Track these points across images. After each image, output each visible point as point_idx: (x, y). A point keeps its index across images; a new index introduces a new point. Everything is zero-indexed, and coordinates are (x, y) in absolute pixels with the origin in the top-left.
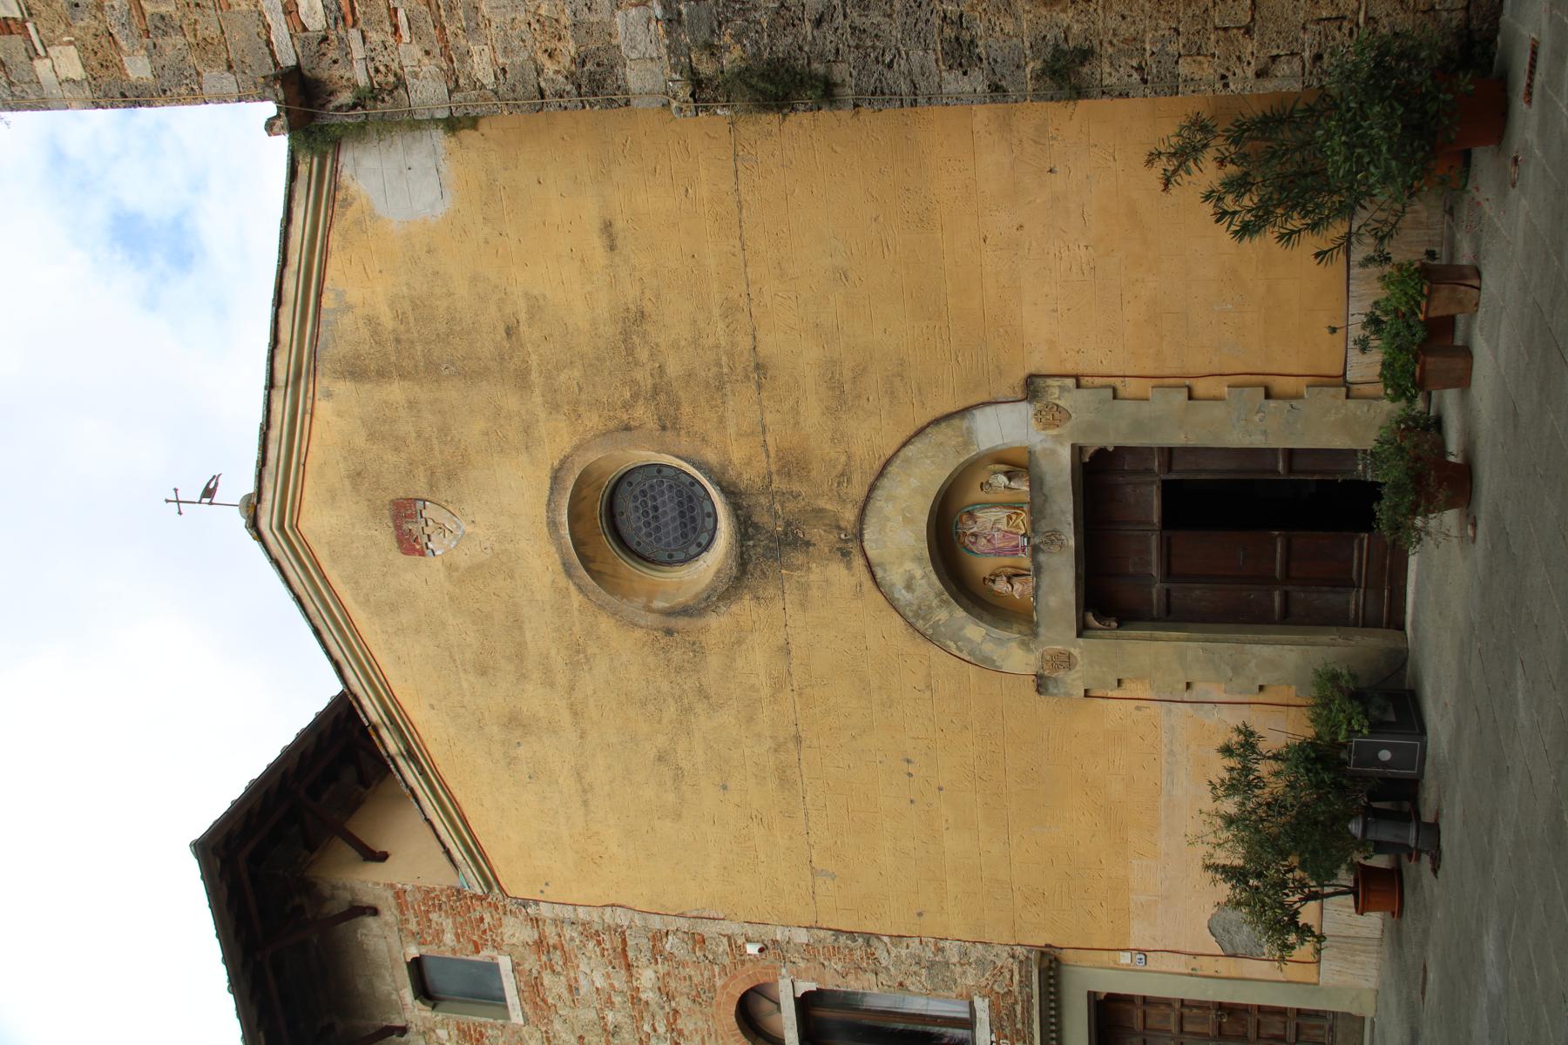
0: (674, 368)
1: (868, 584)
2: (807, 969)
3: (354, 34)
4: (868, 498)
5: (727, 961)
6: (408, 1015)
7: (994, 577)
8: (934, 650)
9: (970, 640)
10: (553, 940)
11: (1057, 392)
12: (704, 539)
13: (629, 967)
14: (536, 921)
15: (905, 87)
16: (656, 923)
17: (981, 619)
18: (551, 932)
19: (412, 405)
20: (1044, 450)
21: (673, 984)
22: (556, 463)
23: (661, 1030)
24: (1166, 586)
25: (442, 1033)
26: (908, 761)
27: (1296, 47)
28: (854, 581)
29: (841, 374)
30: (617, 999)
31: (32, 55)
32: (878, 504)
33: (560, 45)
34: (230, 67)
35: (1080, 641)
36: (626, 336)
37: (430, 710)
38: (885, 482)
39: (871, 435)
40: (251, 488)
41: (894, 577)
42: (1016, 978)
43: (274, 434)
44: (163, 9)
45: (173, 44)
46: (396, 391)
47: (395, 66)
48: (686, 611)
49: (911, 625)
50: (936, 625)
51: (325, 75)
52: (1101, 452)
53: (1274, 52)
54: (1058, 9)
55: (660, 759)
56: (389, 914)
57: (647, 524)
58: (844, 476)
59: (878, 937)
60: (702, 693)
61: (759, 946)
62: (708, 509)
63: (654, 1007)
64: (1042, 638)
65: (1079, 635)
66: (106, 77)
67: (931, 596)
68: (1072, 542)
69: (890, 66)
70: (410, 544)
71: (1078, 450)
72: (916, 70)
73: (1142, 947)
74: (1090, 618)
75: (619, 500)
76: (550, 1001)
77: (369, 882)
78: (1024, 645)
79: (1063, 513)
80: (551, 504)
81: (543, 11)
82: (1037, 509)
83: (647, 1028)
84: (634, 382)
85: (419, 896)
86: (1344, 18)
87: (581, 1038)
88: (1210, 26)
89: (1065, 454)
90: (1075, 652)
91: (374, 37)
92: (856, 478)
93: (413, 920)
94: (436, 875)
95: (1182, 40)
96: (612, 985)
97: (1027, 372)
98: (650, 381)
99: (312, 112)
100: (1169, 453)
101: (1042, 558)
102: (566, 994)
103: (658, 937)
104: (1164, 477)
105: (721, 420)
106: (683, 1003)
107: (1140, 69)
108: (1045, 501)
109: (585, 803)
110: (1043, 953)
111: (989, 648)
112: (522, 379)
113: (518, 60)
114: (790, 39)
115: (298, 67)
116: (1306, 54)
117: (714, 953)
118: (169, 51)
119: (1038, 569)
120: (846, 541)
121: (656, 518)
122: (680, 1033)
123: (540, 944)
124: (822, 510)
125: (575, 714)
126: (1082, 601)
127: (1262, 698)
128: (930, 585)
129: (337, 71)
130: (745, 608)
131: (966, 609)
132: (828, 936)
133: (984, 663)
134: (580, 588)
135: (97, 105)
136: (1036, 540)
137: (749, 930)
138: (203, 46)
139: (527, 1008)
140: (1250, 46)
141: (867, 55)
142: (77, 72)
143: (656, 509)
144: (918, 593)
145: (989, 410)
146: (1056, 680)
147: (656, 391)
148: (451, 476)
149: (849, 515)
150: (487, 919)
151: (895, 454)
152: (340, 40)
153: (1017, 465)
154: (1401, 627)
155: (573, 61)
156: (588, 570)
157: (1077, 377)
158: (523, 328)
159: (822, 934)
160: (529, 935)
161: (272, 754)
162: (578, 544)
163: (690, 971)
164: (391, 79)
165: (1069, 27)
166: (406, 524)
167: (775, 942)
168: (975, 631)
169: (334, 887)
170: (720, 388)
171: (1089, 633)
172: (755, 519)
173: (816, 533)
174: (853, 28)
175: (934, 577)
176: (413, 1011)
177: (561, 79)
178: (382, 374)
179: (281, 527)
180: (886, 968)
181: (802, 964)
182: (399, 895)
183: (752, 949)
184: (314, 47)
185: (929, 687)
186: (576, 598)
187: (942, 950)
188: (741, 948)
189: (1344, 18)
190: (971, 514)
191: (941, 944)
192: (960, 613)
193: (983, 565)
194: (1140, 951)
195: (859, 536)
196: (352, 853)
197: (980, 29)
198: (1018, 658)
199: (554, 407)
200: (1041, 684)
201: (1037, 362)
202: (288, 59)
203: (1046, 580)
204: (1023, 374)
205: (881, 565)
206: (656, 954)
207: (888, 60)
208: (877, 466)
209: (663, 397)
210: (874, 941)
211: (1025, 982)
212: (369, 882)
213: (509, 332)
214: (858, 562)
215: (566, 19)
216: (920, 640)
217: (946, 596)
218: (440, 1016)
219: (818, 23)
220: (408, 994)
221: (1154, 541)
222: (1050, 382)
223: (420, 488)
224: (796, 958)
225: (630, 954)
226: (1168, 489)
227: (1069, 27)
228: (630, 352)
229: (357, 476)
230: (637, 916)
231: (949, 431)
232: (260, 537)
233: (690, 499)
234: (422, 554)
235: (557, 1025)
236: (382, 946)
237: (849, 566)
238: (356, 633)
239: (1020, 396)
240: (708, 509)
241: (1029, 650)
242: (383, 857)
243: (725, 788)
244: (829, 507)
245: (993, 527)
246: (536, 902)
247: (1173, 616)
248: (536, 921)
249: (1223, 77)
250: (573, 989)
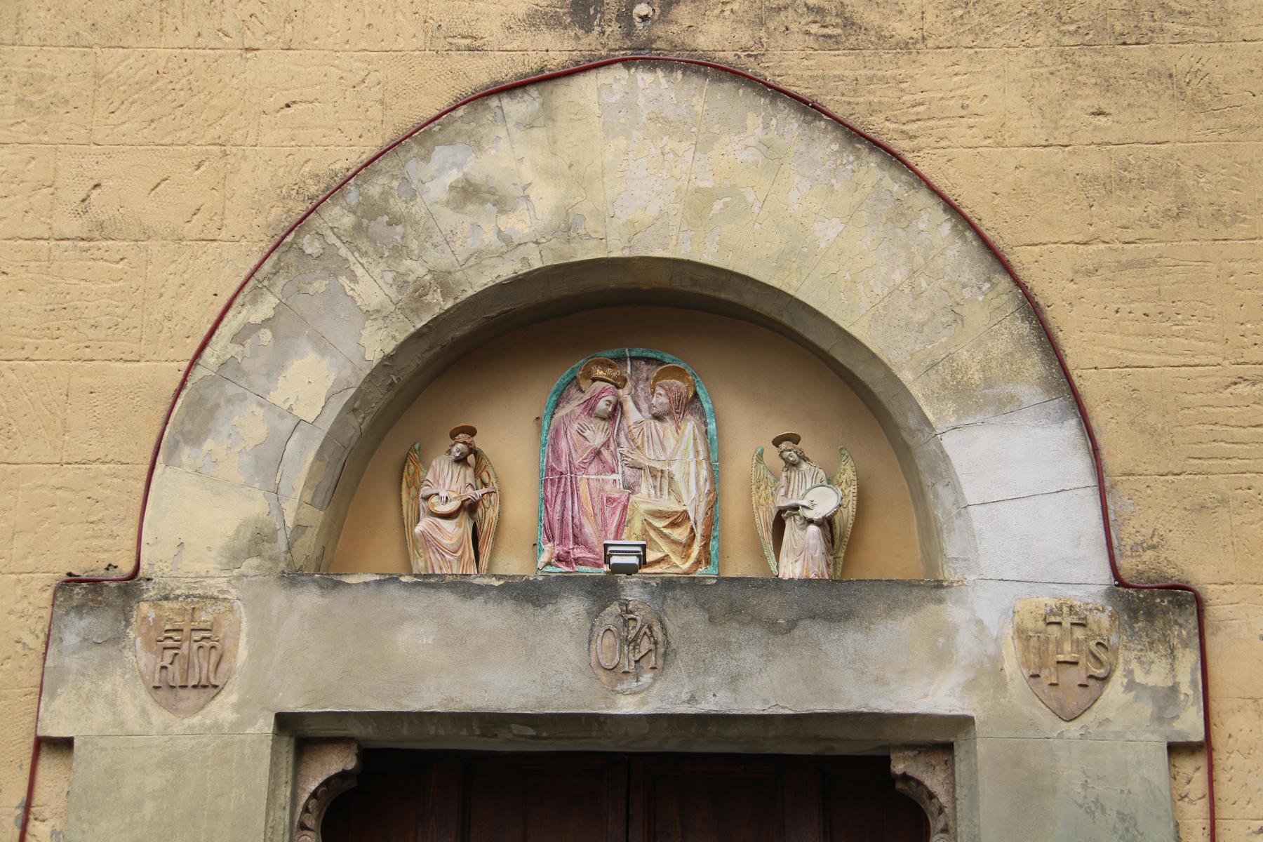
1: (481, 72)
4: (776, 92)
7: (471, 459)
9: (276, 368)
11: (1157, 677)
17: (350, 409)
20: (950, 632)
28: (490, 30)
29: (1180, 39)
32: (754, 121)
35: (266, 726)
38: (828, 145)
41: (508, 149)
49: (336, 190)
50: (332, 266)
58: (842, 30)
64: (279, 598)
65: (285, 722)
67: (443, 260)
68: (627, 706)
71: (942, 738)
74: (338, 762)
78: (258, 540)
79: (733, 681)
82: (739, 601)
89: (935, 696)
90: (223, 708)
92: (839, 63)
97: (1211, 592)
101: (572, 609)
108: (772, 627)
111: (246, 425)
119: (529, 593)
120: (625, 18)
126: (406, 738)
128: (478, 256)
131: (388, 362)
136: (633, 591)
144: (449, 219)
145: (1080, 466)
146: (117, 640)
151: (922, 180)
157: (1204, 748)
168: (312, 385)
171: (287, 758)
175: (506, 270)
185: (101, 231)
190: (689, 404)
192: (377, 343)
195: (641, 57)
200: (101, 594)
203: (494, 618)
204: (1201, 575)
205: (548, 115)
208: (879, 126)
214: (555, 48)
216: (279, 214)
217: (439, 304)
222: (1188, 660)
231: (1001, 345)
239: (1125, 565)
241: (234, 557)
245: (661, 463)
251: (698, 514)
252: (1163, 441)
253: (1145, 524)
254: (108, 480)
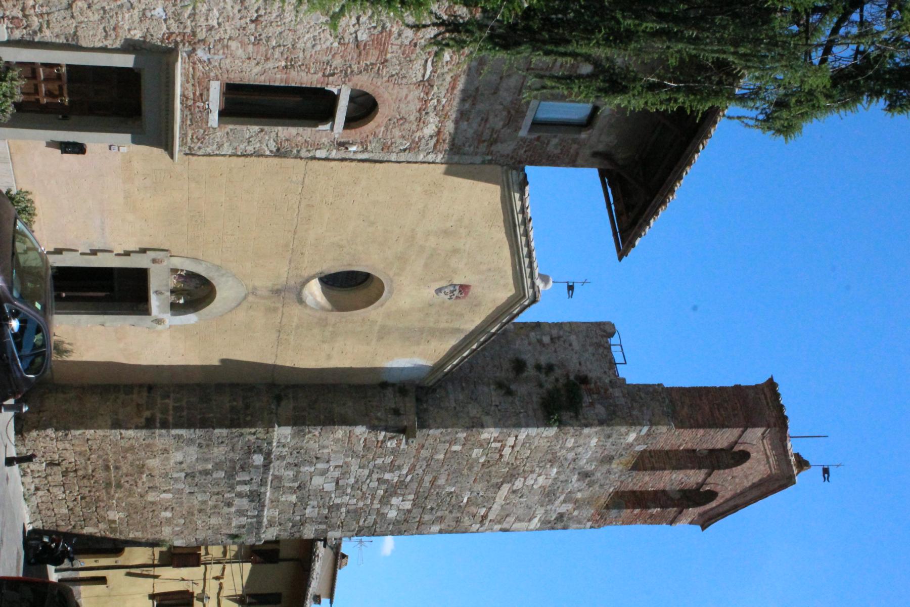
254: (428, 478)
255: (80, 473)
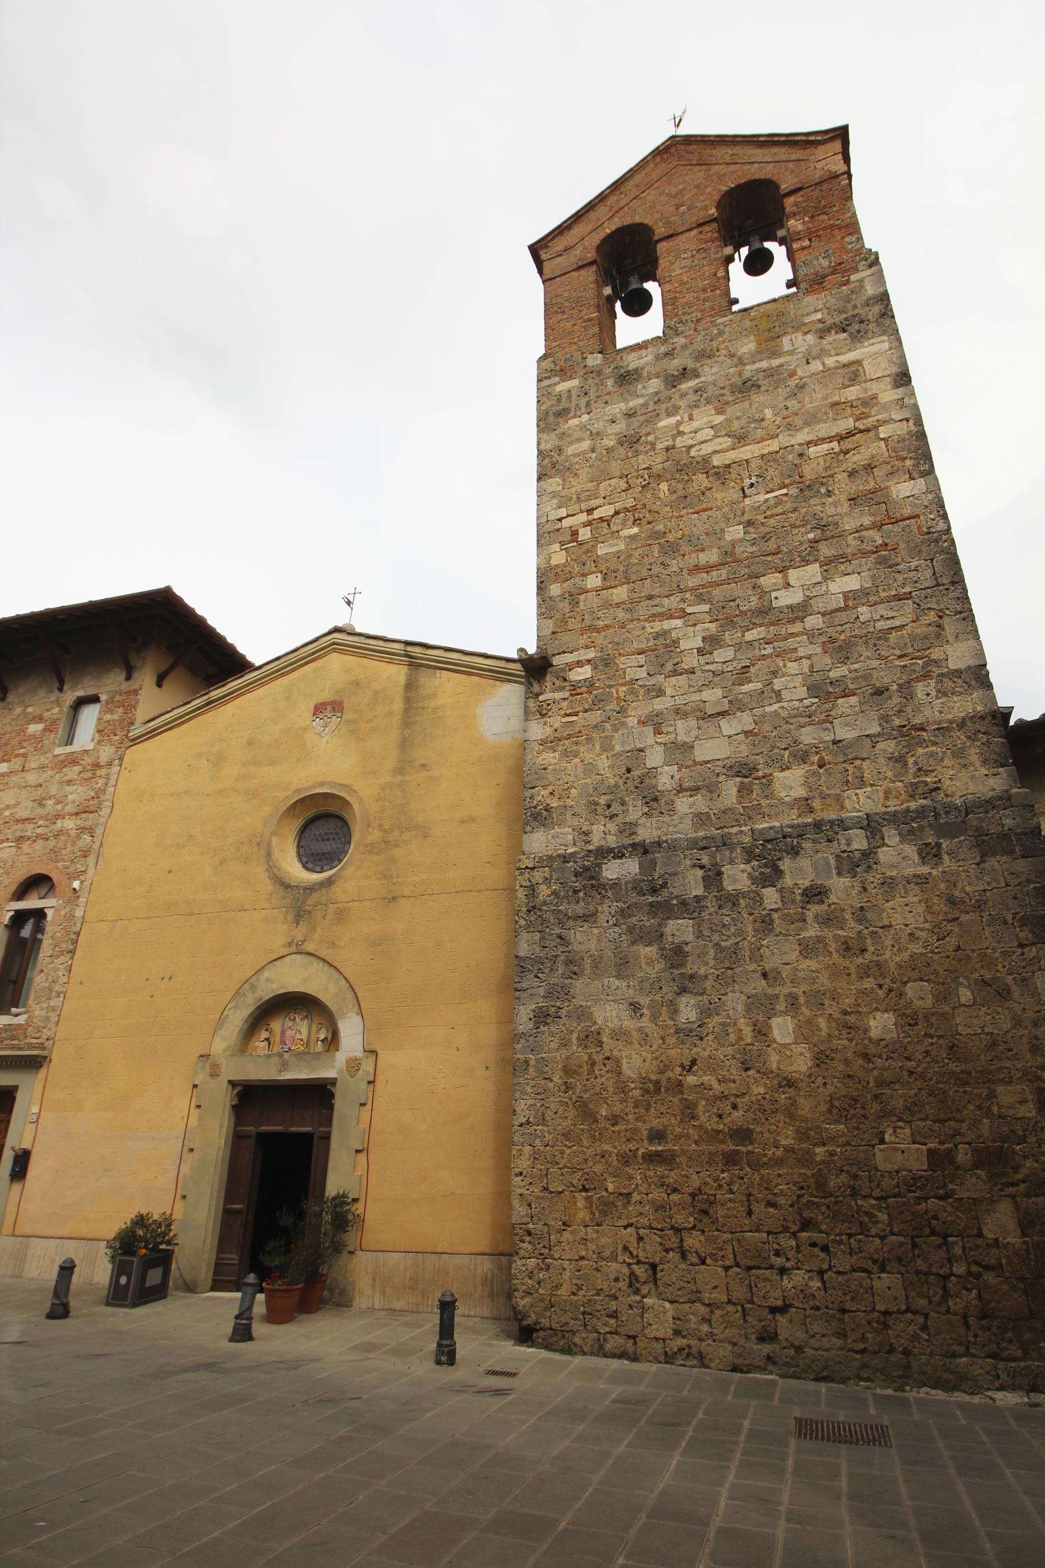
0: (398, 852)
2: (59, 915)
3: (567, 694)
5: (71, 870)
6: (69, 693)
8: (230, 994)
10: (98, 773)
12: (310, 865)
13: (77, 814)
14: (110, 764)
15: (524, 985)
16: (99, 831)
17: (246, 1021)
18: (103, 772)
19: (391, 714)
21: (63, 838)
22: (354, 788)
23: (38, 831)
24: (254, 1136)
25: (56, 710)
26: (170, 978)
27: (535, 1219)
30: (59, 807)
31: (562, 543)
33: (556, 798)
34: (554, 633)
35: (226, 1082)
36: (417, 827)
37: (234, 717)
39: (352, 957)
40: (358, 630)
42: (34, 1041)
43: (381, 643)
44: (581, 603)
45: (565, 607)
46: (398, 705)
47: (550, 713)
48: (269, 854)
51: (548, 679)
52: (332, 1096)
53: (533, 1206)
54: (562, 1074)
55: (190, 836)
56: (125, 686)
57: (320, 835)
58: (332, 945)
59: (72, 958)
60: (223, 861)
61: (77, 888)
62: (325, 868)
63: (53, 827)
66: (551, 575)
69: (536, 977)
70: (319, 709)
71: (333, 1082)
72: (533, 991)
73: (40, 1120)
74: (239, 1089)
75: (332, 821)
76: (65, 769)
77: (145, 678)
80: (333, 784)
81: (573, 790)
83: (41, 822)
84: (392, 831)
85: (133, 703)
86: (550, 1250)
87: (41, 786)
88: (549, 1166)
91: (564, 704)
93: (120, 699)
94: (142, 713)
95: (542, 1149)
96: (67, 804)
98: (391, 839)
99: (535, 669)
100: (327, 1138)
102: (67, 778)
103: (91, 831)
104: (316, 1135)
105: (368, 877)
106: (51, 843)
107: (528, 1122)
109: (171, 795)
110: (46, 1057)
112: (400, 771)
113: (550, 776)
114: (552, 921)
115: (552, 666)
116: (531, 1226)
117: (77, 863)
118: (562, 605)
121: (323, 840)
122: (35, 841)
123: (97, 766)
124: (315, 930)
125: (221, 791)
127: (178, 1197)
129: (549, 684)
130: (267, 886)
131: (251, 1014)
132: (76, 929)
133: (221, 1021)
134: (287, 797)
135: (538, 569)
137: (87, 883)
138: (564, 621)
139: (62, 757)
140: (537, 1190)
141: (542, 964)
142: (554, 561)
143: (328, 840)
147: (386, 842)
148: (353, 732)
149: (310, 947)
150: (116, 738)
152: (564, 688)
153: (333, 1041)
154: (213, 1289)
155: (548, 805)
156: (296, 802)
158: (425, 773)
159: (79, 925)
160: (103, 761)
161: (221, 630)
162: (311, 797)
163: (69, 848)
164: (544, 712)
165: (551, 1081)
166: (328, 708)
167: (78, 897)
168: (238, 1018)
169: (144, 659)
170: (385, 877)
172: (314, 894)
173: (303, 928)
174: (556, 956)
176: (70, 696)
177: (540, 798)
178: (408, 700)
179: (334, 644)
180: (52, 963)
181: (63, 912)
182: (135, 692)
183: (76, 884)
184: (561, 674)
186: (282, 795)
187: (58, 995)
188: (77, 878)
189: (550, 1250)
191: (62, 995)
192: (251, 1010)
193: (276, 1025)
194: (38, 1119)
196: (163, 668)
197: (554, 1028)
198: (219, 1046)
199: (383, 787)
201: (384, 1057)
202: (556, 661)
206: (82, 829)
207: (540, 975)
209: (383, 845)
210: (69, 955)
211: (32, 1046)
212: (145, 678)
213: (423, 765)
214: (285, 951)
215: (569, 802)
218: (65, 710)
219: (560, 937)
220: (80, 693)
221: (280, 1128)
223: (348, 715)
224: (68, 909)
225: (84, 815)
226: (309, 1136)
227: (551, 1081)
228: (408, 830)
229: (357, 684)
230: (104, 820)
232: (330, 633)
233: (331, 858)
234: (314, 714)
235: (50, 773)
236: (110, 681)
237: (284, 946)
238: (276, 678)
240: (325, 868)
242: (159, 684)
243: (170, 872)
244: (317, 936)
245: (298, 1029)
246: (121, 765)
247: (237, 1139)
248: (110, 764)
249: (521, 1174)
250: (69, 782)
251: (305, 1039)
252: (693, 884)
253: (831, 1306)
255: (681, 1219)
